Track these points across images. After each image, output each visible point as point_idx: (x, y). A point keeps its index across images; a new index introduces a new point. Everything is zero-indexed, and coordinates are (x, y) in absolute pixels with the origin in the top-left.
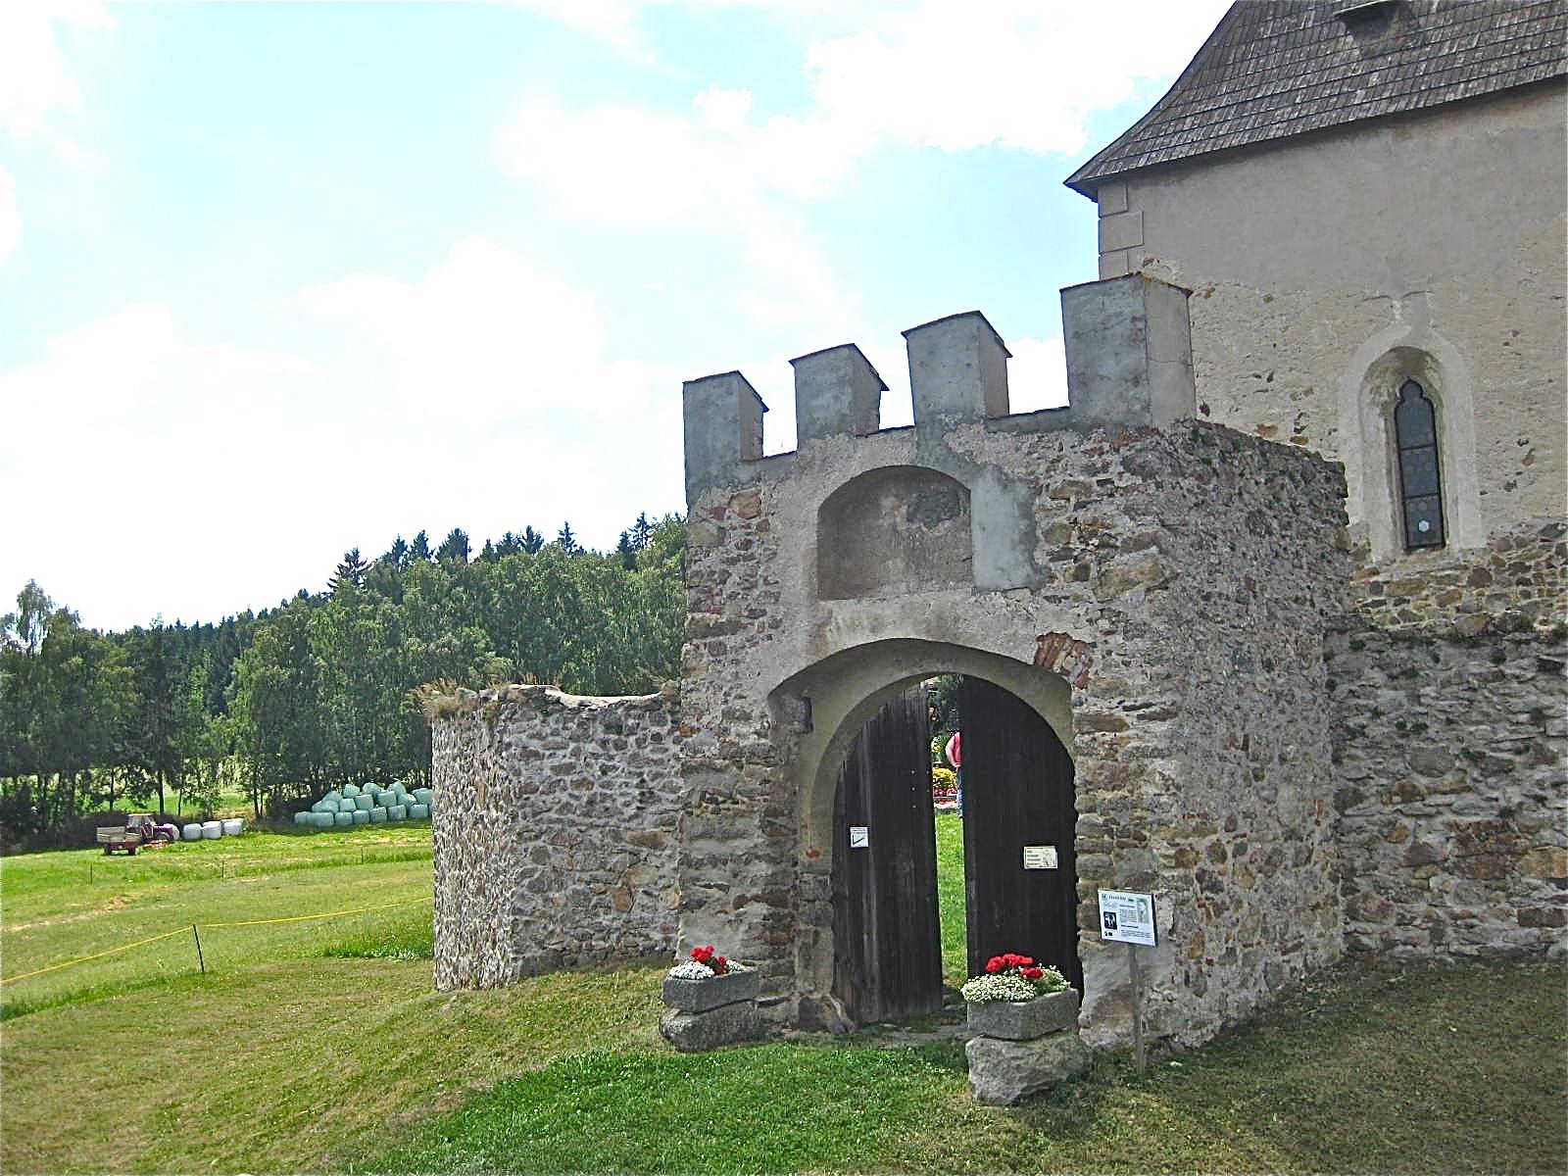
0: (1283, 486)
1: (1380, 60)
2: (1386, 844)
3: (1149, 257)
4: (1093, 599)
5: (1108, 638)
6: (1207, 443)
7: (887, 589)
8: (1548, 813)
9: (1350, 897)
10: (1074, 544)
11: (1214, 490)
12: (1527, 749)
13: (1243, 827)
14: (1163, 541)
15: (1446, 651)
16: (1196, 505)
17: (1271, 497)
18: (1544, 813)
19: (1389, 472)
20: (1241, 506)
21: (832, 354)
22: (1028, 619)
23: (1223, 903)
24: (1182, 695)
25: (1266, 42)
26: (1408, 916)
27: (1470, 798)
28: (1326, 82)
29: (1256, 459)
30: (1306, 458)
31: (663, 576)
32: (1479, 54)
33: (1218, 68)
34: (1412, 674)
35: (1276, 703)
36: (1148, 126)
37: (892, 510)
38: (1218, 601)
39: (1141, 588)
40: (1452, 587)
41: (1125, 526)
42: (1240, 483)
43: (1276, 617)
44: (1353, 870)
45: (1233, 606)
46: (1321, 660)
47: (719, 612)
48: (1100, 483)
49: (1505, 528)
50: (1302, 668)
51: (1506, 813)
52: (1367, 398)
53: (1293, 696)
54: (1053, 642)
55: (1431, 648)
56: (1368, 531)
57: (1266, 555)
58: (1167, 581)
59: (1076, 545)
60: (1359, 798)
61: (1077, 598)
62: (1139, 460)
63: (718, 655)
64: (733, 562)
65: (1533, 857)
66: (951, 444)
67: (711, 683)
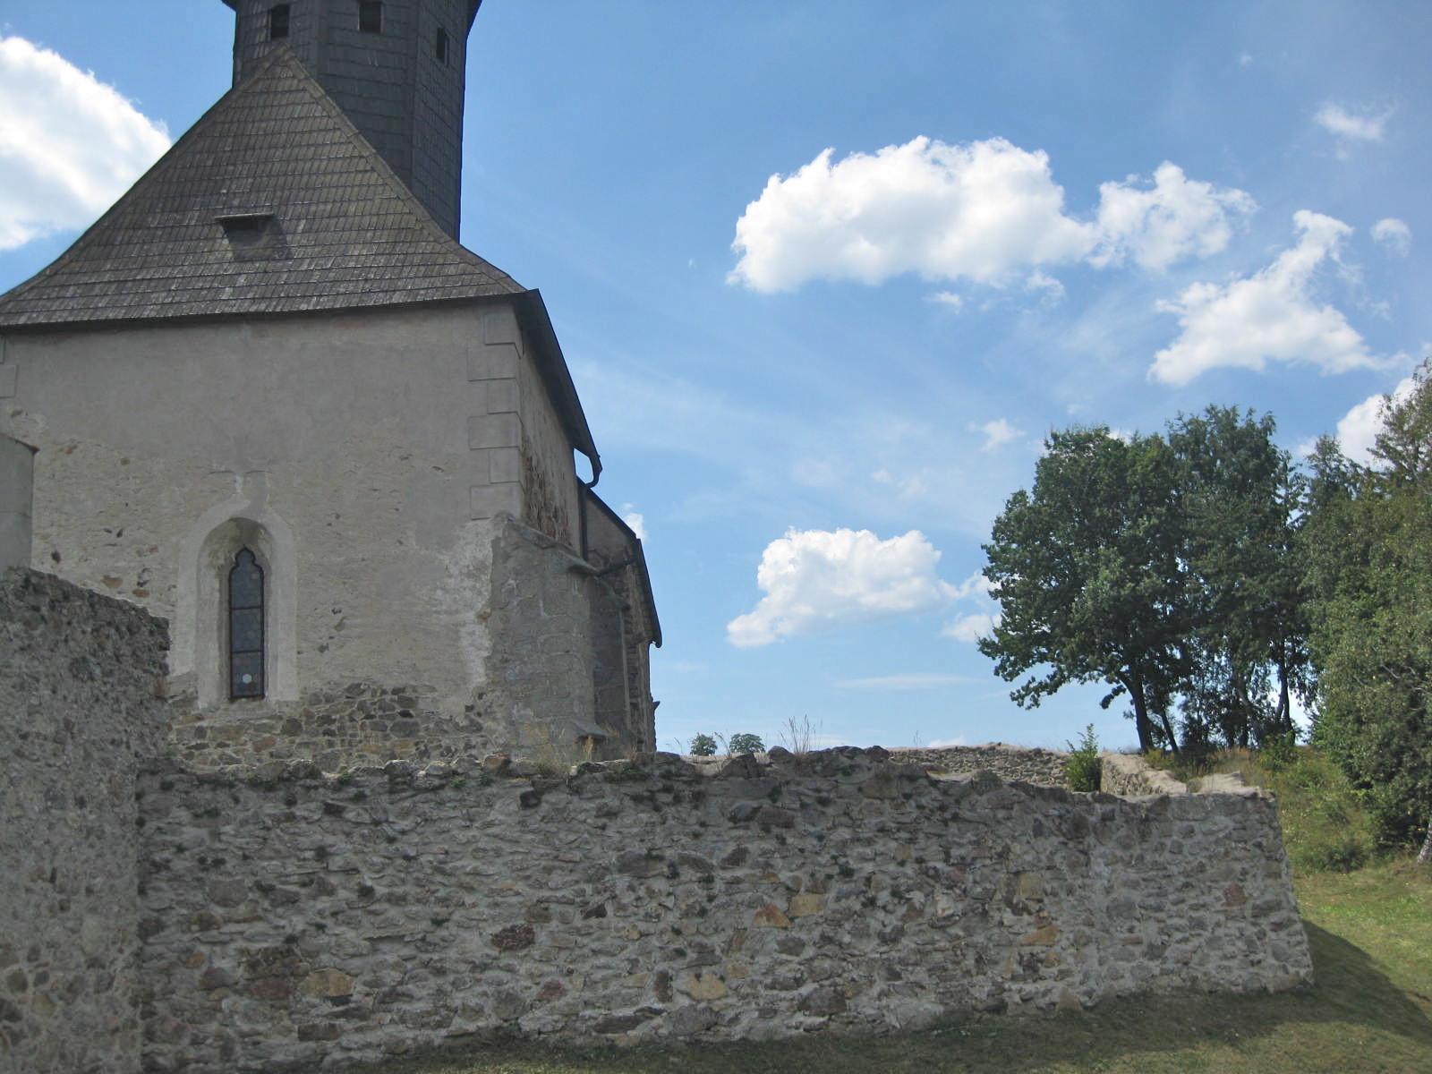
0: (108, 637)
1: (249, 265)
2: (183, 970)
3: (18, 408)
6: (38, 590)
8: (326, 939)
9: (148, 1020)
12: (312, 882)
13: (46, 956)
15: (246, 794)
18: (323, 939)
19: (219, 628)
23: (21, 1031)
26: (201, 1036)
27: (260, 926)
29: (85, 609)
32: (332, 275)
35: (87, 838)
36: (32, 288)
40: (268, 735)
42: (66, 631)
44: (152, 995)
45: (49, 746)
49: (317, 685)
50: (113, 805)
51: (291, 939)
53: (103, 831)
60: (159, 926)
65: (312, 978)
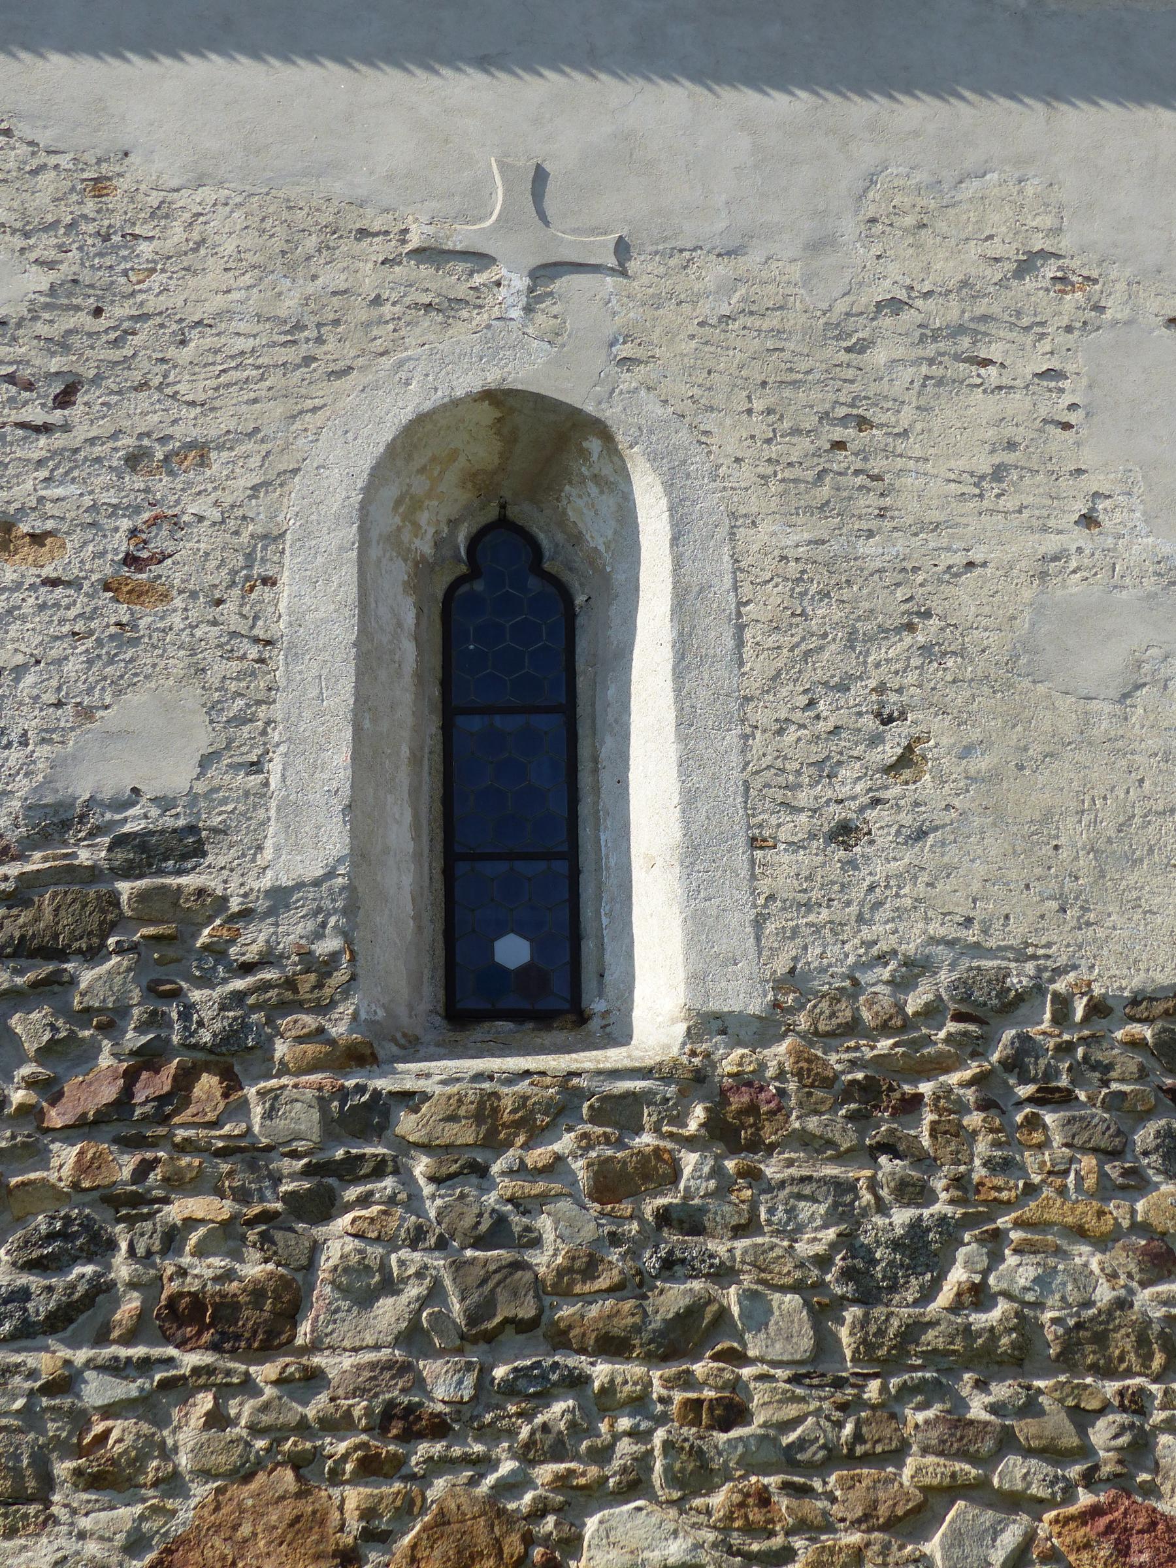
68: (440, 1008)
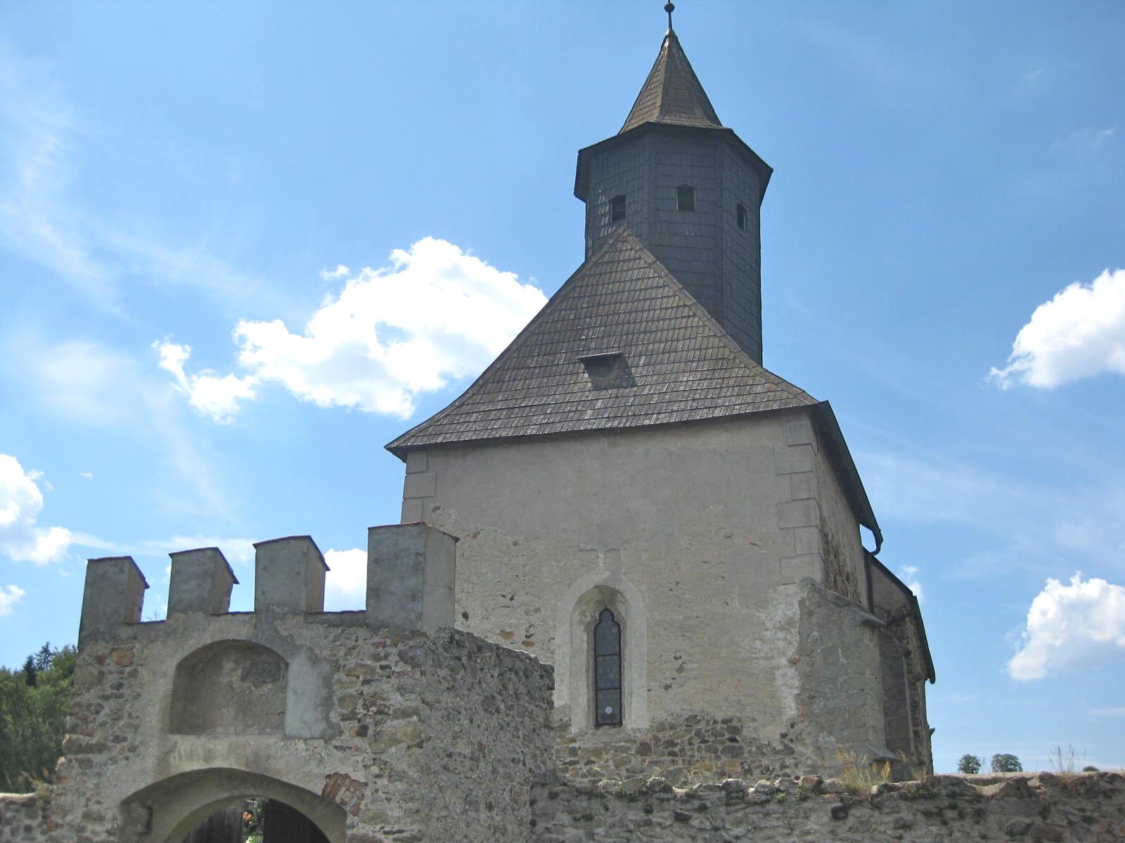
0: (510, 680)
1: (604, 392)
4: (369, 750)
5: (377, 780)
6: (460, 645)
7: (220, 730)
10: (359, 709)
11: (461, 679)
14: (422, 713)
15: (614, 804)
16: (448, 689)
17: (501, 687)
19: (587, 670)
20: (480, 692)
21: (200, 554)
22: (321, 761)
24: (426, 825)
25: (532, 370)
28: (568, 402)
30: (528, 661)
31: (56, 693)
33: (498, 382)
34: (589, 818)
35: (494, 834)
36: (446, 416)
37: (231, 673)
38: (458, 759)
39: (403, 745)
40: (625, 755)
41: (396, 700)
43: (498, 772)
45: (468, 763)
46: (528, 805)
47: (91, 735)
48: (382, 667)
49: (662, 716)
50: (514, 809)
52: (576, 618)
53: (506, 829)
54: (337, 780)
55: (603, 800)
56: (570, 711)
57: (494, 728)
58: (422, 742)
59: (361, 711)
61: (357, 749)
62: (411, 654)
63: (86, 768)
64: (106, 698)
66: (279, 628)
67: (77, 790)
68: (595, 724)
